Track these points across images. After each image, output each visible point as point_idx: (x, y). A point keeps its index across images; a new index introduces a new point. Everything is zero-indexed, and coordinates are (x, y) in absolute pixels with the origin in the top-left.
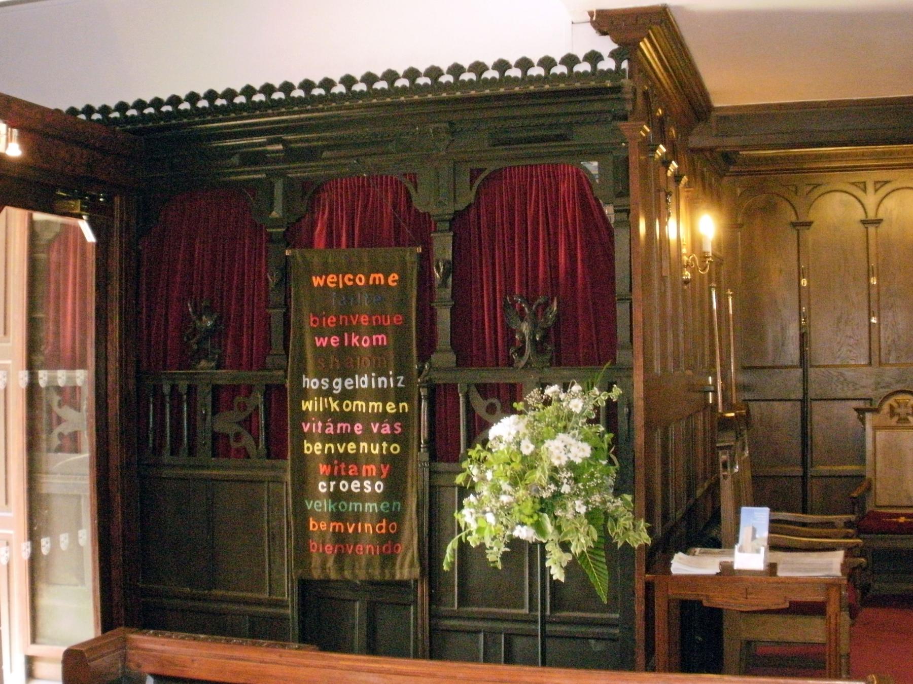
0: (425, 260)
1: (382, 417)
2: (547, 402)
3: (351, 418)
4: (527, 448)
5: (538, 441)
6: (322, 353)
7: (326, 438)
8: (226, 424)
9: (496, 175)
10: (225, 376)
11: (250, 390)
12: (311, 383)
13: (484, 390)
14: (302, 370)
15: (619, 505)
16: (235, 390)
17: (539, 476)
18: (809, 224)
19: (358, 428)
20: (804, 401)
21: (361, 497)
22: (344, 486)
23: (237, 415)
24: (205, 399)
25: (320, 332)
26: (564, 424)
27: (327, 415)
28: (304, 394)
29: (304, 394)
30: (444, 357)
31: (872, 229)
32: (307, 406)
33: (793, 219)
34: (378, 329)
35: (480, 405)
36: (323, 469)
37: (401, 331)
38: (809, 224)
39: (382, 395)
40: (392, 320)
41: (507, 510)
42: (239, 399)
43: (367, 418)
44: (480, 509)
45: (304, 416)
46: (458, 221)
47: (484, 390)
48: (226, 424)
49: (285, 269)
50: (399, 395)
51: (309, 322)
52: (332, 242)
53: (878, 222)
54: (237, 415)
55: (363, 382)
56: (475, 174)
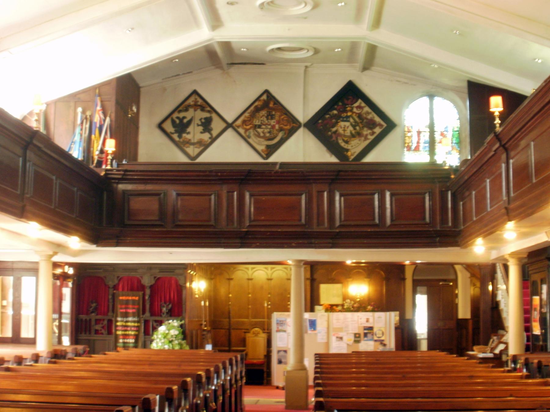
0: (144, 295)
1: (134, 326)
2: (169, 324)
3: (127, 326)
4: (167, 332)
5: (169, 330)
6: (122, 313)
7: (122, 331)
8: (98, 327)
9: (159, 278)
10: (99, 317)
11: (104, 320)
12: (119, 319)
13: (156, 321)
14: (117, 316)
15: (184, 342)
16: (100, 320)
17: (169, 337)
18: (232, 279)
19: (129, 329)
20: (229, 329)
21: (129, 343)
22: (126, 341)
23: (101, 325)
24: (93, 322)
25: (121, 308)
26: (173, 327)
27: (123, 326)
28: (117, 321)
29: (117, 321)
30: (148, 314)
31: (250, 281)
32: (119, 324)
33: (228, 277)
34: (134, 308)
35: (155, 324)
36: (121, 337)
37: (138, 310)
38: (232, 279)
39: (134, 322)
40: (136, 307)
41: (164, 342)
42: (101, 322)
43: (131, 327)
44: (157, 343)
45: (116, 326)
46: (151, 287)
47: (156, 321)
48: (98, 327)
49: (114, 295)
50: (138, 322)
51: (119, 306)
52: (123, 290)
53: (251, 279)
54: (101, 325)
55: (130, 319)
56: (155, 277)
